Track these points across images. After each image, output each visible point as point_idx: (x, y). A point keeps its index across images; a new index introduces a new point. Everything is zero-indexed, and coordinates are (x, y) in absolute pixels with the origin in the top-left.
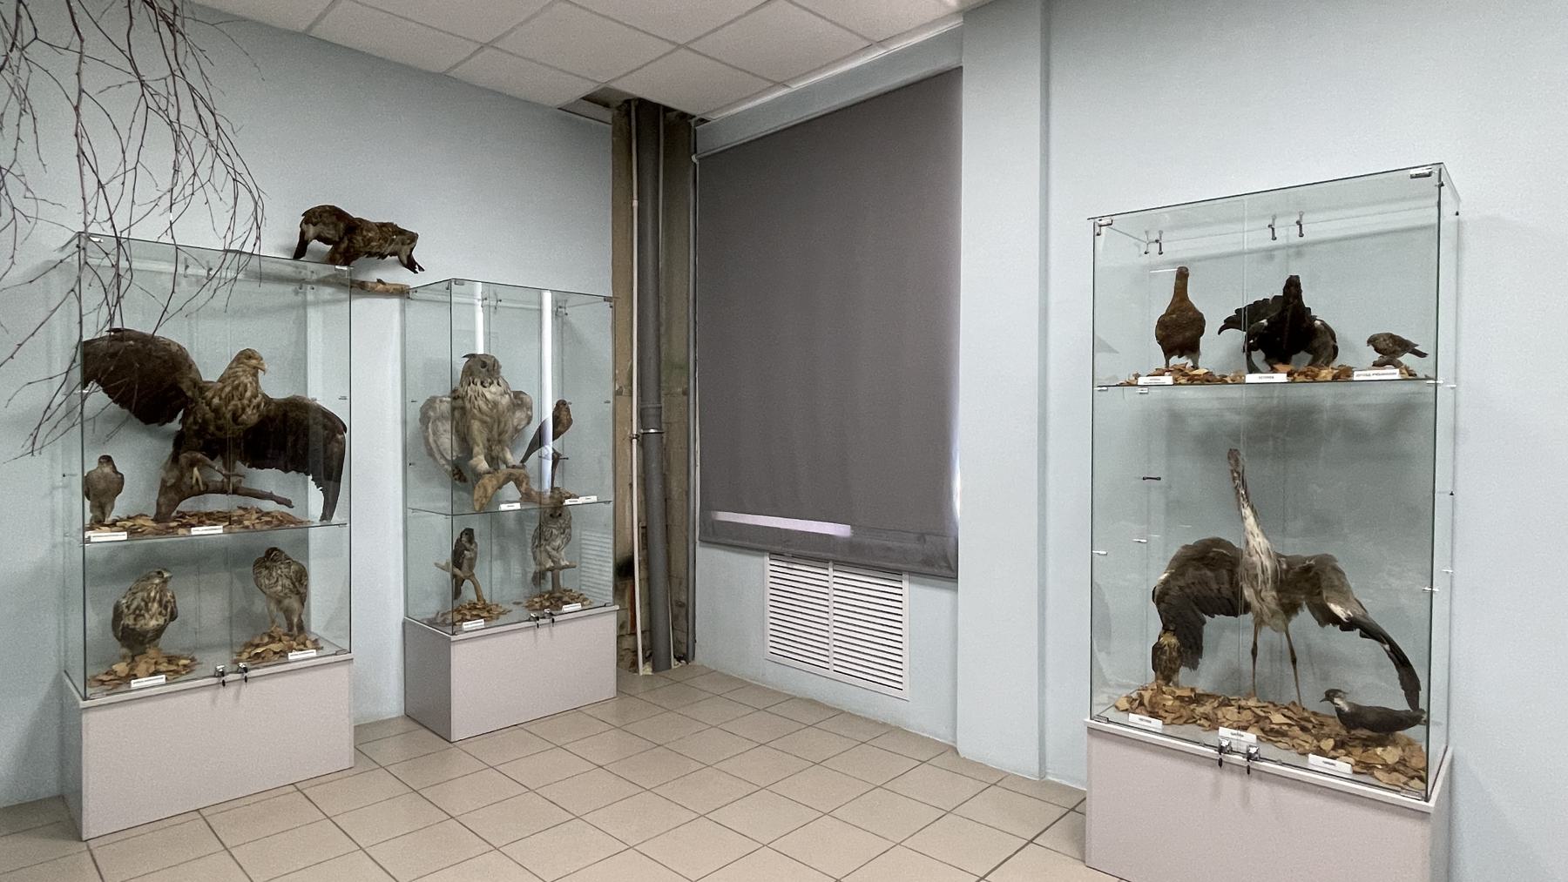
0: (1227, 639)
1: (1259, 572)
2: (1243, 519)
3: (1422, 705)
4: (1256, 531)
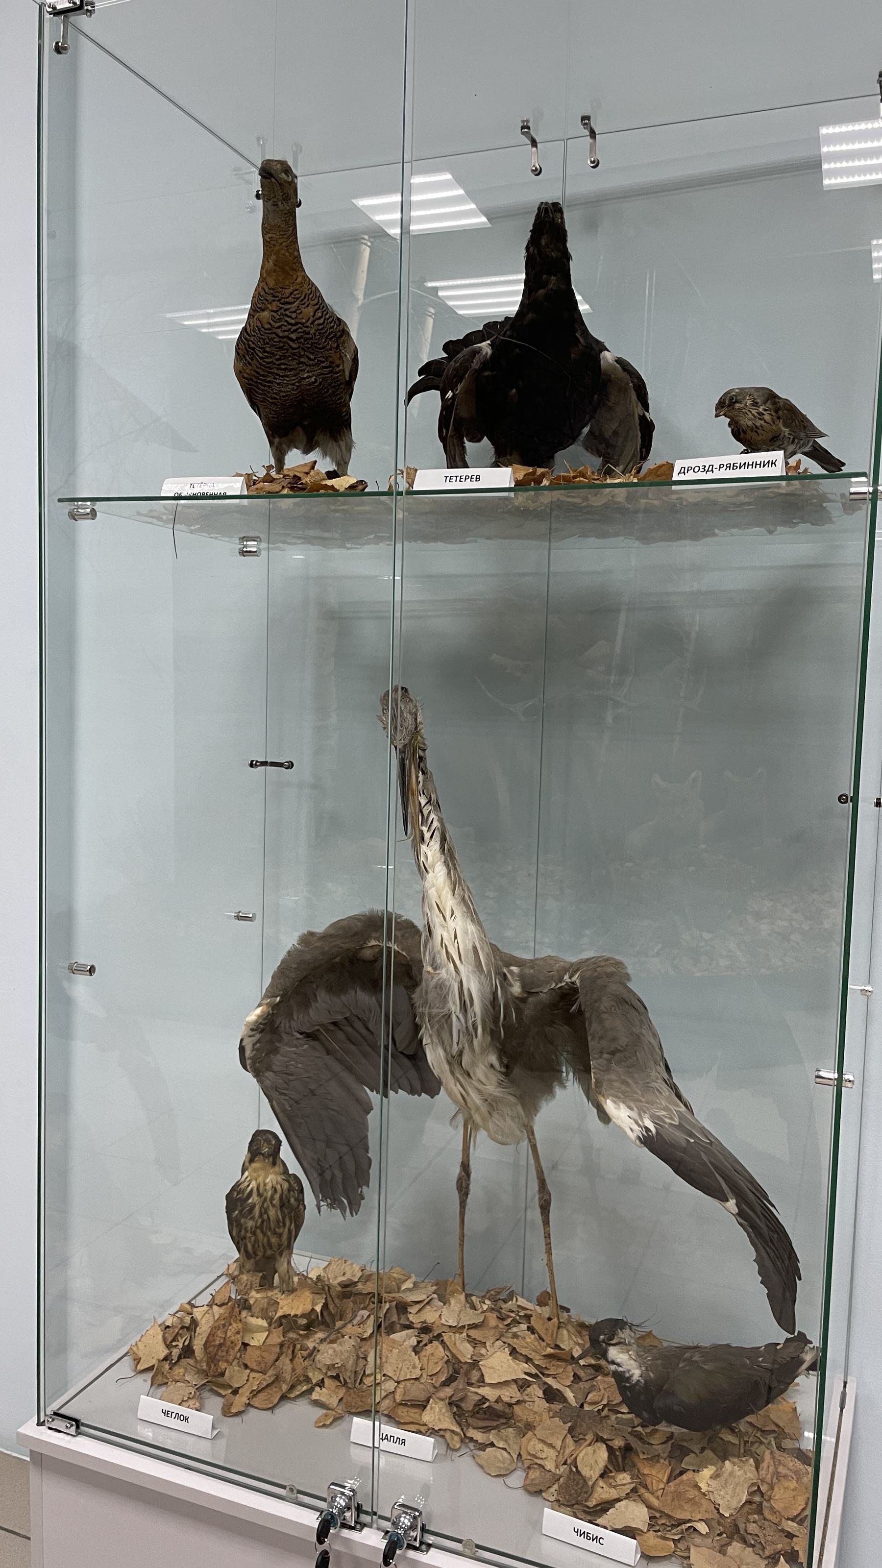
0: (419, 1137)
1: (454, 1006)
2: (422, 870)
3: (807, 1319)
4: (450, 902)
